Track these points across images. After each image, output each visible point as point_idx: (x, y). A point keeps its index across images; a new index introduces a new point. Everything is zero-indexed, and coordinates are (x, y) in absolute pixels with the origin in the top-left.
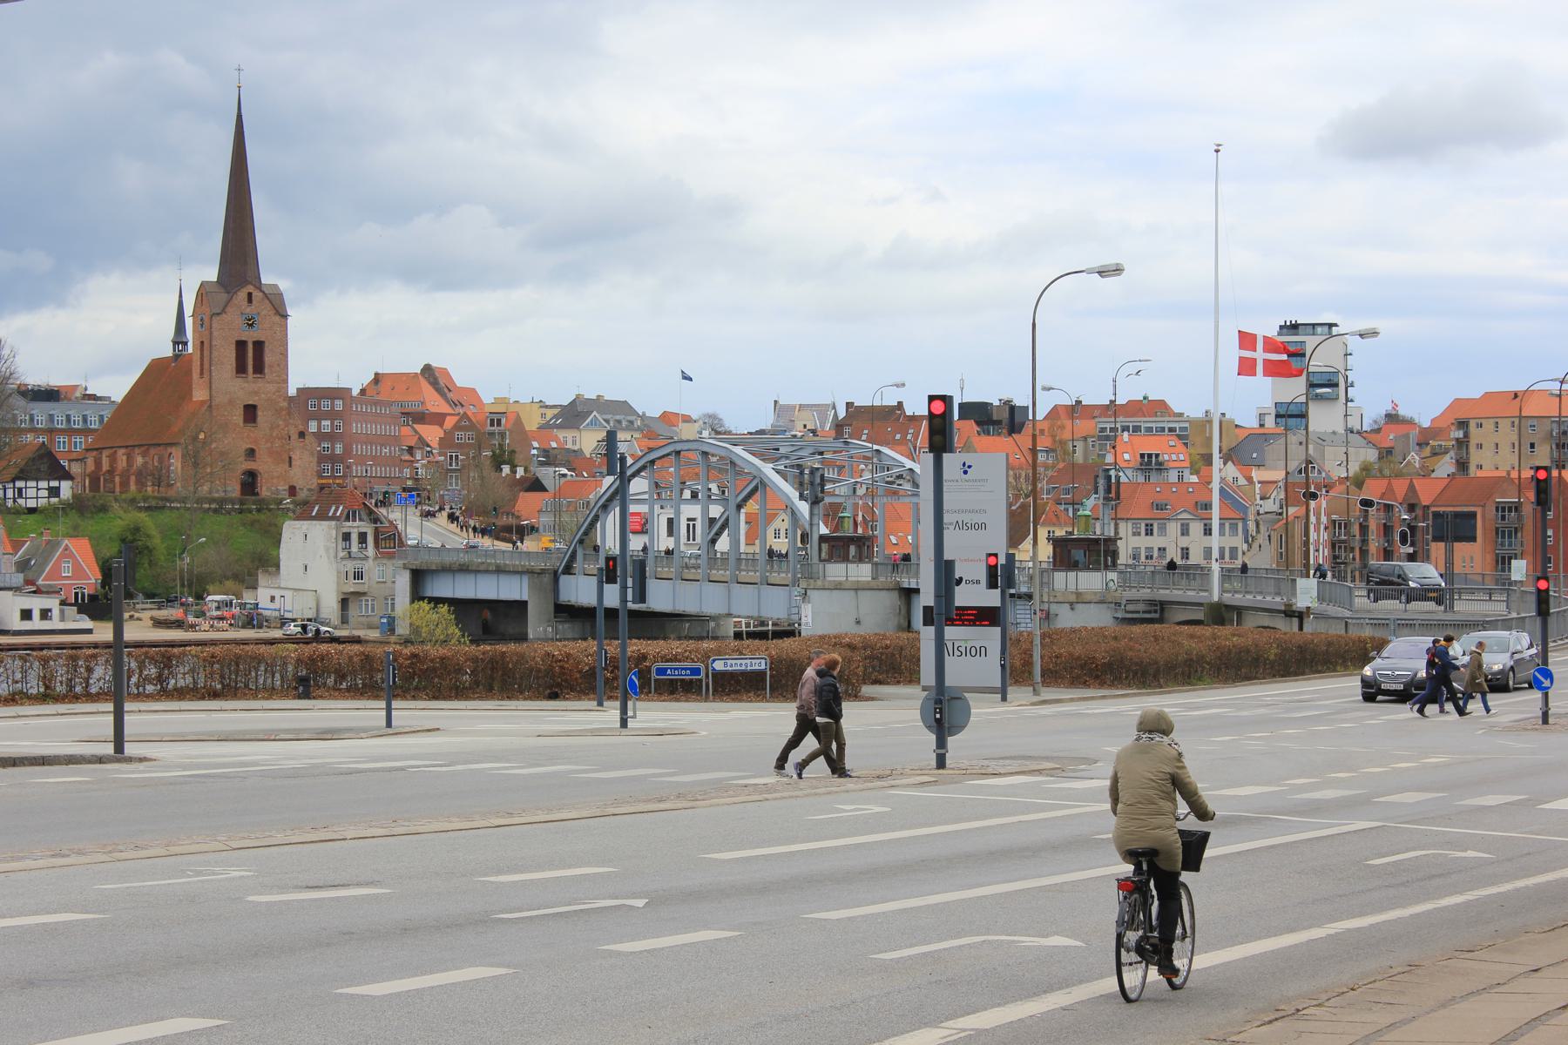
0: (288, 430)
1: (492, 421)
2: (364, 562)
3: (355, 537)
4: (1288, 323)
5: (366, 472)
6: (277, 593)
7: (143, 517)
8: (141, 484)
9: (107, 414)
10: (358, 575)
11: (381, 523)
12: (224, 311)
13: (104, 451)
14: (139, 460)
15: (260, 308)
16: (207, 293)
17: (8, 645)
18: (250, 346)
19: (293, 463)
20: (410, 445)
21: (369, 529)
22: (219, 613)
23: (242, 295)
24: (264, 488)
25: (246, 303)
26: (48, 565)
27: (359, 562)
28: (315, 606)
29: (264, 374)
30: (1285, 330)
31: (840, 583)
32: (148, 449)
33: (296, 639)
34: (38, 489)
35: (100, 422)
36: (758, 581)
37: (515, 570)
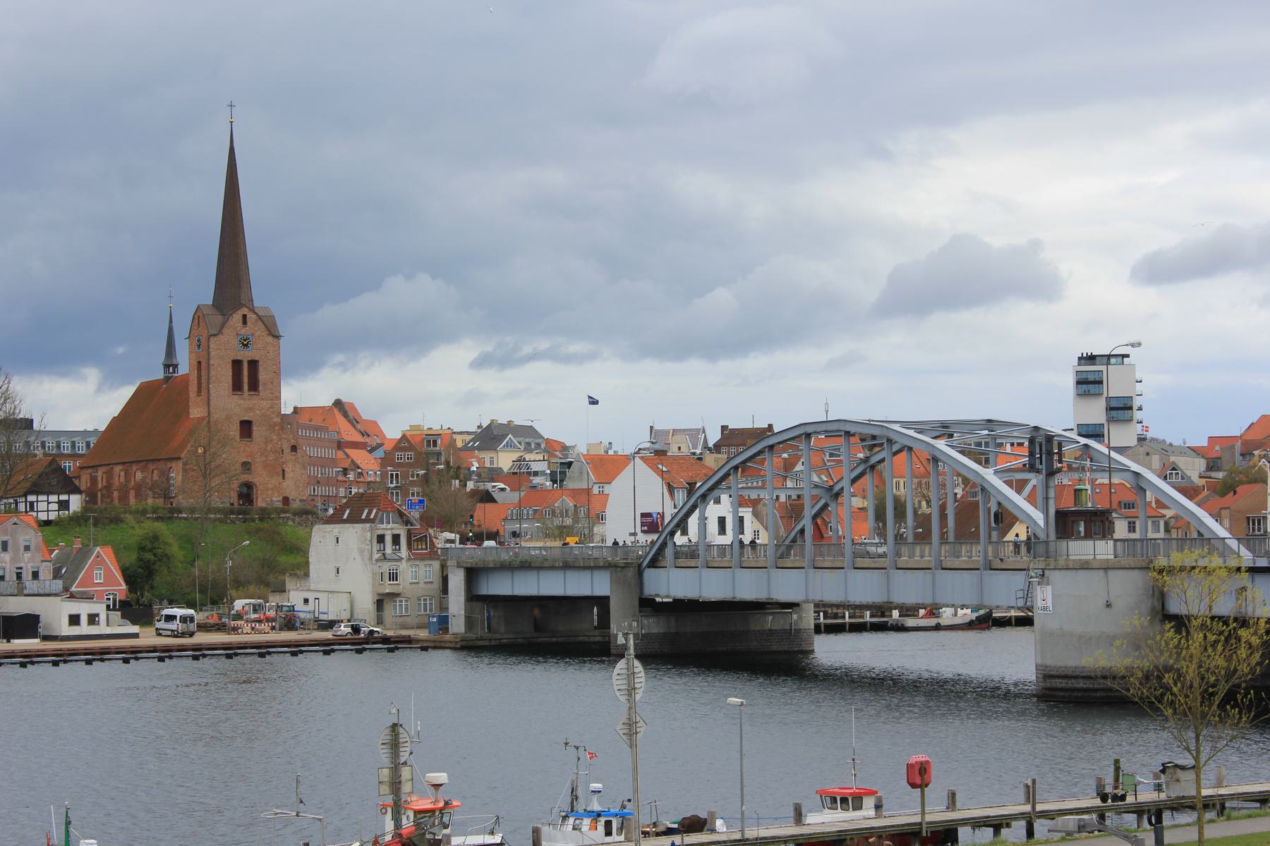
1: (429, 442)
2: (398, 563)
3: (388, 539)
4: (1085, 355)
5: (314, 491)
9: (93, 440)
10: (394, 576)
12: (220, 332)
13: (99, 468)
14: (139, 475)
15: (255, 330)
16: (204, 315)
18: (245, 365)
19: (286, 475)
20: (344, 467)
22: (256, 616)
23: (237, 317)
24: (259, 500)
25: (241, 324)
27: (394, 563)
30: (1083, 361)
31: (1087, 562)
32: (147, 464)
34: (49, 503)
35: (72, 447)
36: (932, 565)
37: (587, 564)
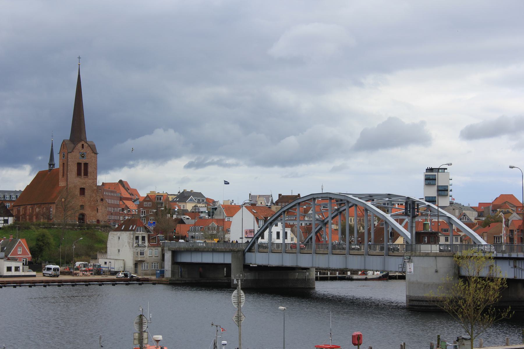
0: (97, 198)
2: (144, 248)
3: (140, 238)
4: (429, 168)
6: (107, 261)
7: (45, 231)
8: (37, 218)
9: (19, 195)
10: (142, 254)
11: (150, 233)
12: (72, 151)
14: (37, 210)
16: (66, 144)
17: (6, 281)
19: (99, 211)
20: (123, 208)
21: (146, 235)
22: (85, 269)
23: (80, 145)
26: (12, 250)
27: (142, 248)
28: (123, 266)
29: (88, 176)
30: (428, 171)
31: (428, 253)
33: (122, 279)
35: (10, 198)
36: (364, 253)
